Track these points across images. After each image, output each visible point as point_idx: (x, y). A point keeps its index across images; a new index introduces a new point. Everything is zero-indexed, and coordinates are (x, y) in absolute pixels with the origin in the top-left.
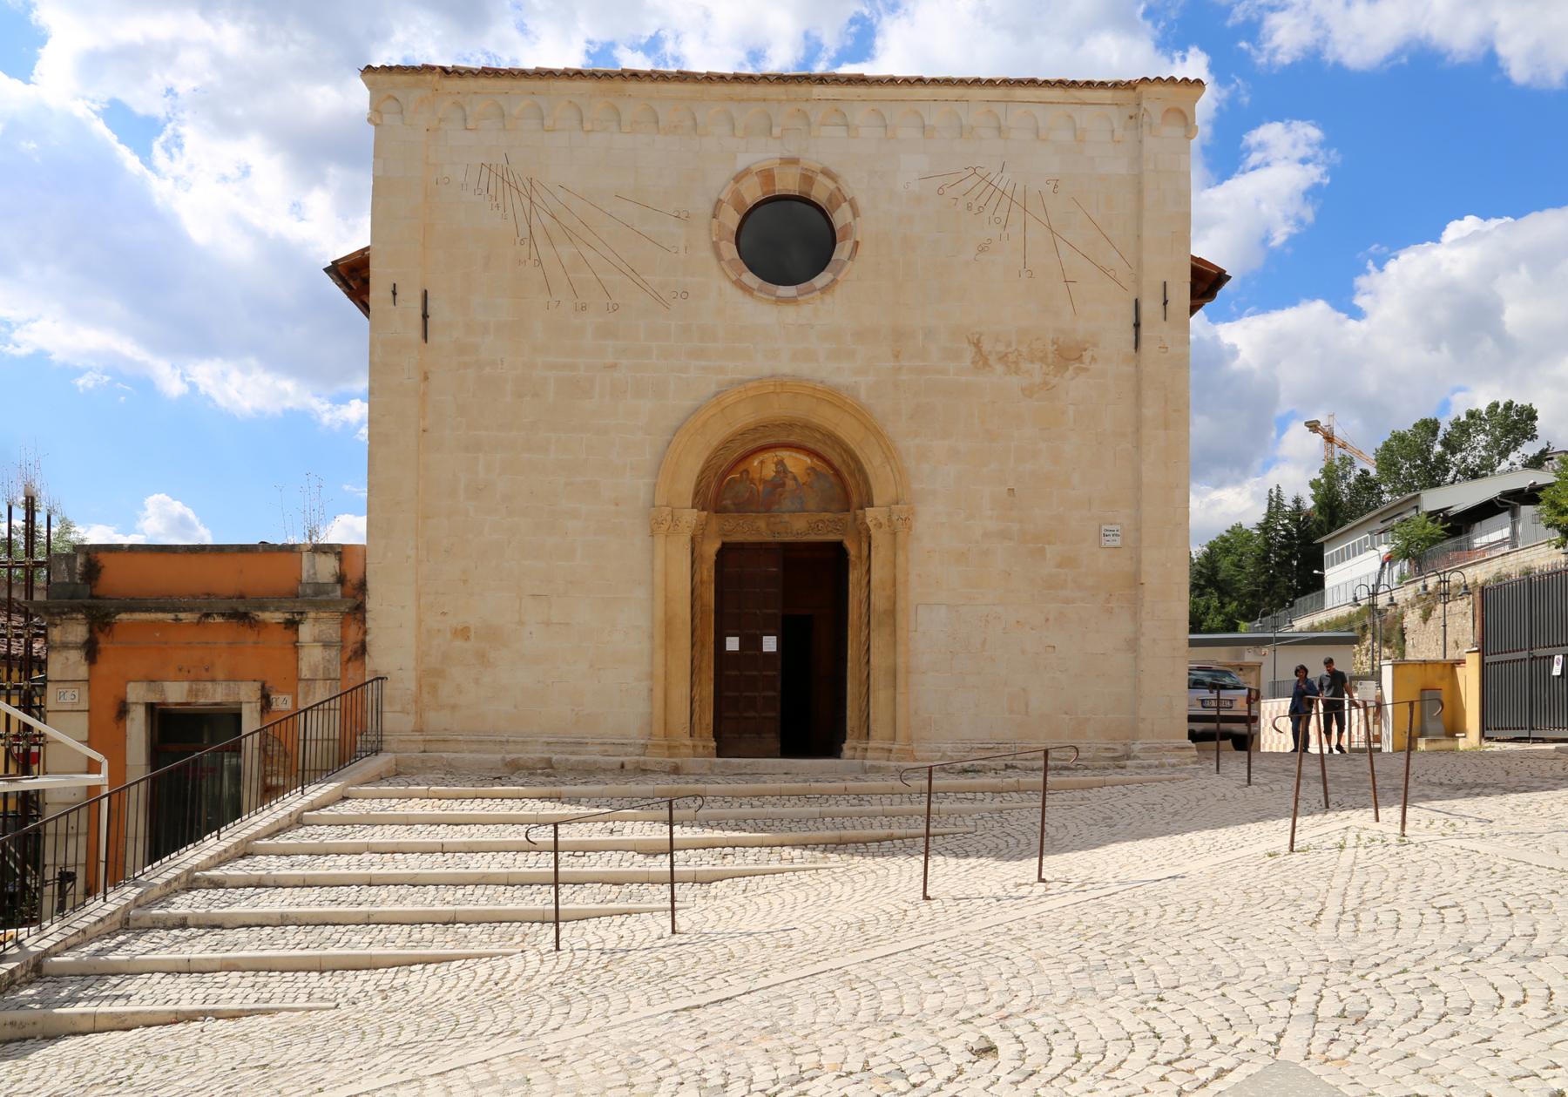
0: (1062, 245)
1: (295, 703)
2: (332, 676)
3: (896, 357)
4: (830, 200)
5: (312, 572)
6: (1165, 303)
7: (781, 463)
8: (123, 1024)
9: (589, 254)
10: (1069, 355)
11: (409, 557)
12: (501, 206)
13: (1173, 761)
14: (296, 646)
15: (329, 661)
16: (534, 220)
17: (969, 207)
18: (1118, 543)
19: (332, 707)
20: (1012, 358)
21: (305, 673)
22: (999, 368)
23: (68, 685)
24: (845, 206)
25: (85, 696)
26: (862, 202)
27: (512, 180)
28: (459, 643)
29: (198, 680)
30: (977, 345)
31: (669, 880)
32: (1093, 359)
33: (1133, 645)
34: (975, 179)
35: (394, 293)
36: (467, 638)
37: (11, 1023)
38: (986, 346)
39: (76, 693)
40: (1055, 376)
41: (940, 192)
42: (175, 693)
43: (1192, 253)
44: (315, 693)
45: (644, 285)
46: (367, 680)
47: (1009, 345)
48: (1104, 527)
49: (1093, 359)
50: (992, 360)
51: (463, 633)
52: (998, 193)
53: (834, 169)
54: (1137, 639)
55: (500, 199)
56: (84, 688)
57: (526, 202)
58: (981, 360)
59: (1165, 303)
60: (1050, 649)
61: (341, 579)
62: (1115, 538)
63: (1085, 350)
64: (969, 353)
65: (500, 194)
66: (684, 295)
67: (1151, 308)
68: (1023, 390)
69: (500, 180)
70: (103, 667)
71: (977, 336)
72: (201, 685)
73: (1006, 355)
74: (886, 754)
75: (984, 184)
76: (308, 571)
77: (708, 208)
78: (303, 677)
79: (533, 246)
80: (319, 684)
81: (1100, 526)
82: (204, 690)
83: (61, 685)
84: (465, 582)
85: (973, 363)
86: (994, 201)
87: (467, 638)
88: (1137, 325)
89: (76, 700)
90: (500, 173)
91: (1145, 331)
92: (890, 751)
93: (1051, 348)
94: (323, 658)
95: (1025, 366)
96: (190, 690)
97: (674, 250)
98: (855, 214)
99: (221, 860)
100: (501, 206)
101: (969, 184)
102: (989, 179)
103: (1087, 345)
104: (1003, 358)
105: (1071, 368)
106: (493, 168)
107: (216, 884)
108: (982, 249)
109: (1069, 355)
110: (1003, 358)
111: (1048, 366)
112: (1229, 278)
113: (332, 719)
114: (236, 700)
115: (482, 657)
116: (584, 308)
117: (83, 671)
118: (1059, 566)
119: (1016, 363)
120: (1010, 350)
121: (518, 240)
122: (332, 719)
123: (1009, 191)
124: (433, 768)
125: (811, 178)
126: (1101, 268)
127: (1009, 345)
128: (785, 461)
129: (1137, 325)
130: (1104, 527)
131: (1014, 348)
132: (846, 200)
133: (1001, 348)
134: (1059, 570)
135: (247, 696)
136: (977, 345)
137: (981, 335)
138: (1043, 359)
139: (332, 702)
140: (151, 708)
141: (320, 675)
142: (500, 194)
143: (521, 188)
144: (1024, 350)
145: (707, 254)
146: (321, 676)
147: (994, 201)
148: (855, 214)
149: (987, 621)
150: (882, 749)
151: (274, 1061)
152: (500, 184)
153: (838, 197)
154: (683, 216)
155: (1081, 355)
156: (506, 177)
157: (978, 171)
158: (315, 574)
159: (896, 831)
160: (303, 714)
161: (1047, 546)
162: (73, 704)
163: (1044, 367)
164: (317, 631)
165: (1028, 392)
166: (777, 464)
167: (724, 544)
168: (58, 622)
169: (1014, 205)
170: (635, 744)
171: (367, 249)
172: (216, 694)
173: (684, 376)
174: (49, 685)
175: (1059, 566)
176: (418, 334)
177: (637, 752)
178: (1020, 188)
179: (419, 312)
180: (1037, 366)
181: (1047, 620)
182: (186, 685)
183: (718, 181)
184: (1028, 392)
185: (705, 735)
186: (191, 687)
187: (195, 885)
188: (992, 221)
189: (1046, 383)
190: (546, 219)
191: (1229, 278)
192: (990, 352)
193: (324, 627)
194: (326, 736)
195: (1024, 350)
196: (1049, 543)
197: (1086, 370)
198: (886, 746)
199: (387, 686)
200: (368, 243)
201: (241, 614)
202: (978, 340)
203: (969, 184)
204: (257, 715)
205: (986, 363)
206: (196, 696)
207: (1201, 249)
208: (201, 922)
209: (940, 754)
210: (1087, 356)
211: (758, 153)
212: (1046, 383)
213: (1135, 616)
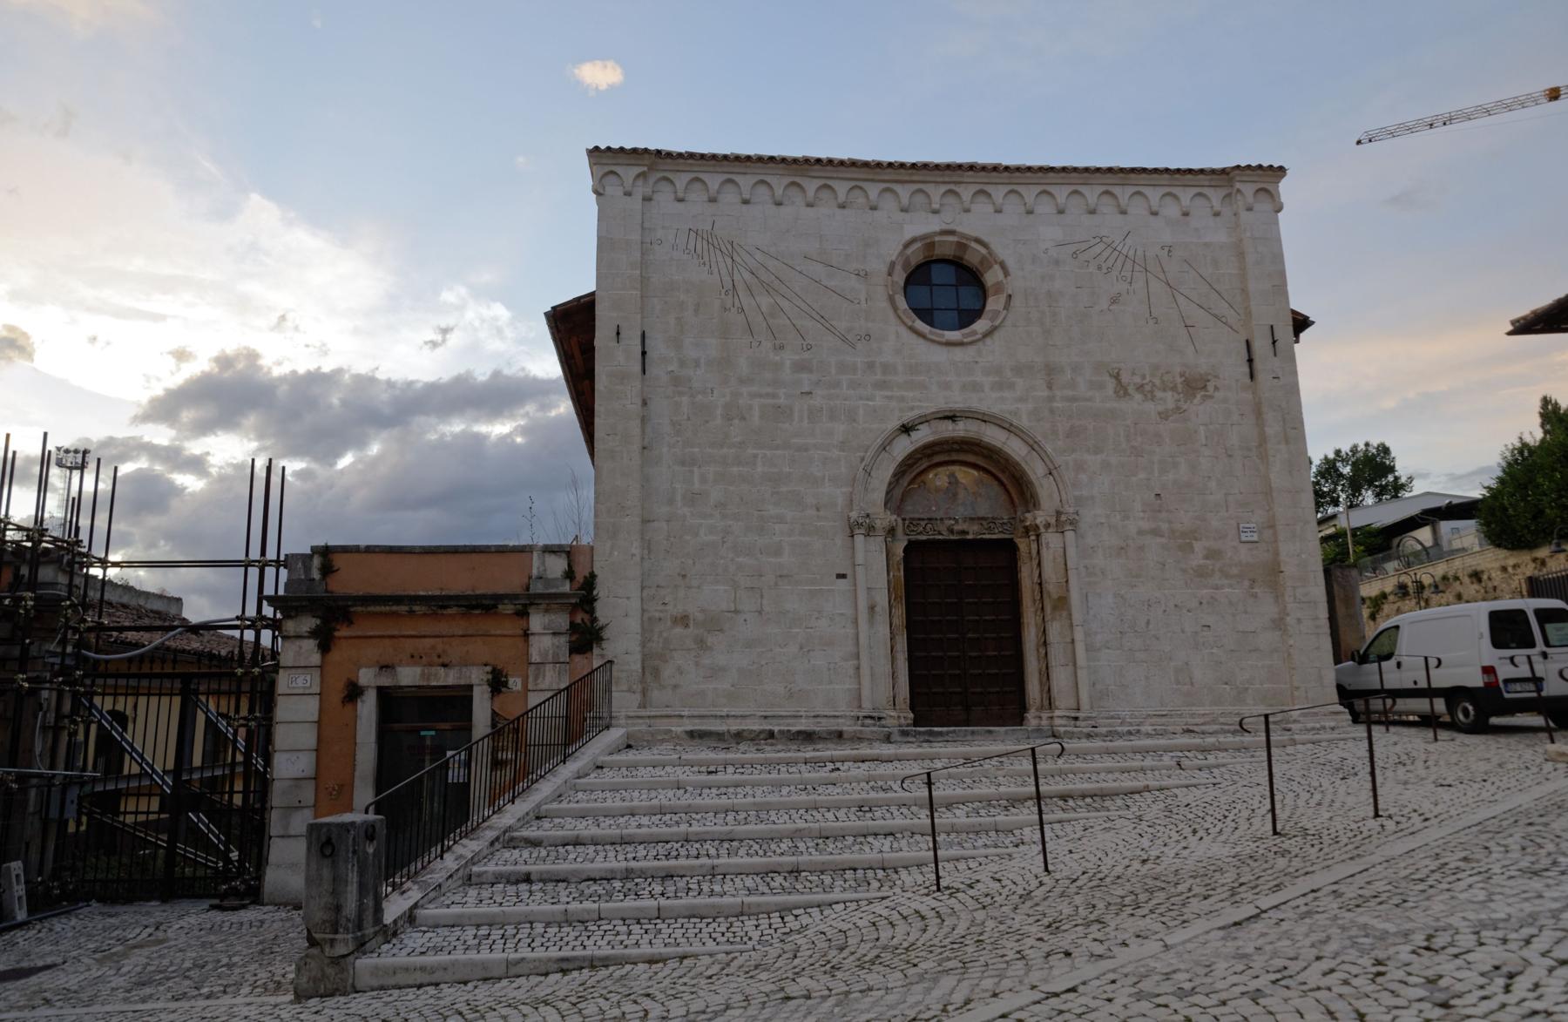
0: (1181, 299)
2: (562, 660)
3: (1050, 387)
4: (981, 263)
5: (541, 569)
6: (1274, 342)
7: (952, 475)
8: (430, 980)
9: (785, 304)
10: (1195, 385)
11: (633, 555)
12: (707, 263)
13: (1333, 724)
14: (526, 635)
15: (558, 647)
18: (1255, 538)
20: (1148, 388)
21: (535, 658)
22: (1138, 397)
23: (300, 671)
25: (317, 680)
26: (1011, 263)
27: (716, 243)
28: (679, 630)
29: (431, 665)
30: (1117, 377)
31: (930, 832)
32: (1216, 388)
33: (1279, 624)
34: (1102, 246)
35: (618, 334)
36: (687, 626)
37: (421, 969)
38: (1125, 378)
39: (308, 678)
40: (1186, 402)
41: (1075, 255)
42: (408, 676)
43: (1292, 307)
44: (544, 676)
45: (833, 330)
46: (595, 667)
47: (1144, 377)
48: (1241, 525)
49: (1216, 388)
50: (1131, 390)
51: (683, 620)
52: (1122, 258)
53: (985, 239)
54: (1282, 619)
55: (706, 259)
56: (317, 673)
57: (729, 261)
58: (1122, 391)
59: (1274, 342)
60: (1205, 629)
61: (569, 575)
63: (1209, 381)
64: (1111, 385)
65: (706, 253)
66: (867, 338)
67: (1261, 346)
68: (1159, 413)
69: (705, 243)
70: (335, 655)
72: (433, 670)
73: (1142, 386)
74: (1073, 722)
75: (1109, 250)
76: (538, 568)
77: (885, 269)
78: (533, 661)
79: (736, 297)
80: (550, 666)
81: (1238, 524)
82: (436, 675)
83: (293, 671)
84: (684, 576)
85: (1115, 392)
86: (1119, 263)
87: (687, 626)
88: (1250, 361)
89: (308, 684)
91: (1258, 364)
92: (1076, 719)
93: (1179, 380)
94: (553, 644)
95: (1159, 394)
96: (423, 675)
97: (856, 301)
98: (1006, 274)
99: (524, 821)
100: (707, 263)
101: (1097, 249)
102: (1114, 245)
103: (1209, 377)
104: (1140, 388)
105: (1199, 396)
106: (700, 232)
107: (535, 843)
108: (1114, 301)
109: (1195, 385)
110: (1140, 388)
111: (1179, 394)
112: (1313, 323)
114: (468, 682)
115: (701, 643)
116: (782, 347)
117: (316, 658)
118: (1206, 557)
120: (1144, 382)
121: (723, 291)
123: (1131, 253)
124: (663, 741)
125: (965, 245)
126: (1215, 316)
127: (1144, 377)
128: (957, 474)
129: (1250, 361)
132: (996, 262)
133: (1138, 380)
134: (1208, 562)
135: (477, 677)
136: (1117, 377)
137: (1120, 370)
138: (1174, 389)
140: (381, 691)
141: (550, 659)
142: (706, 253)
143: (723, 249)
144: (1157, 382)
145: (884, 304)
146: (551, 660)
147: (1119, 263)
148: (1006, 274)
149: (1149, 606)
150: (1068, 717)
151: (865, 955)
152: (705, 246)
153: (989, 260)
154: (862, 273)
155: (1206, 386)
157: (1104, 239)
158: (545, 570)
159: (1152, 783)
161: (1194, 542)
162: (304, 688)
163: (1176, 396)
164: (547, 621)
165: (1164, 416)
166: (949, 477)
167: (910, 542)
168: (293, 614)
169: (1137, 268)
170: (846, 716)
171: (593, 294)
172: (449, 678)
173: (871, 403)
174: (281, 671)
175: (1206, 557)
176: (638, 368)
177: (848, 723)
178: (1140, 253)
179: (639, 349)
180: (1170, 394)
181: (1201, 603)
182: (418, 670)
183: (891, 248)
184: (1164, 416)
185: (903, 706)
186: (423, 671)
187: (512, 844)
189: (1178, 408)
190: (747, 276)
191: (1313, 323)
193: (553, 617)
195: (1157, 382)
196: (1196, 539)
197: (1211, 397)
198: (1073, 715)
199: (615, 668)
200: (594, 289)
201: (482, 605)
202: (1118, 373)
203: (1097, 249)
204: (487, 695)
205: (1126, 393)
206: (428, 679)
207: (1296, 305)
208: (545, 876)
210: (1210, 386)
211: (923, 225)
212: (1178, 408)
213: (1278, 597)
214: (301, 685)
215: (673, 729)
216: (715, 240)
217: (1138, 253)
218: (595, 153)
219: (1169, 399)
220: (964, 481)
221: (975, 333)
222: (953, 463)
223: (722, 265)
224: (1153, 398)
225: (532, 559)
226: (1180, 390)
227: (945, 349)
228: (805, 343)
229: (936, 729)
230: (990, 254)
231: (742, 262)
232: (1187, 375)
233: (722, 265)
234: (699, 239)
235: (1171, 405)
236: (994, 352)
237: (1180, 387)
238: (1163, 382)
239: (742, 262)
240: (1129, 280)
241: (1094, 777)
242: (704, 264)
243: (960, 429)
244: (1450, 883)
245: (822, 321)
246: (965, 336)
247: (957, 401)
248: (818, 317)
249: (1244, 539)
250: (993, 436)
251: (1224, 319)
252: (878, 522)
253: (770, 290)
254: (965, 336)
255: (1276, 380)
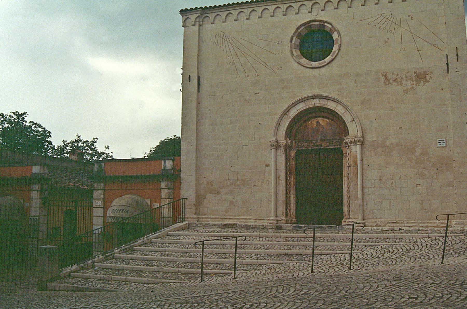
1: (160, 204)
7: (318, 122)
16: (232, 51)
17: (380, 28)
18: (444, 145)
19: (167, 207)
20: (399, 80)
24: (335, 33)
30: (386, 76)
34: (382, 18)
38: (389, 76)
57: (230, 44)
60: (418, 185)
62: (443, 143)
63: (427, 74)
64: (383, 79)
66: (281, 69)
71: (385, 73)
78: (162, 198)
86: (389, 25)
89: (100, 205)
90: (221, 36)
104: (395, 80)
105: (422, 82)
111: (413, 81)
113: (165, 214)
119: (400, 81)
122: (165, 214)
130: (438, 139)
131: (399, 76)
132: (335, 31)
133: (394, 76)
136: (386, 76)
139: (167, 205)
144: (404, 76)
147: (389, 25)
153: (334, 29)
155: (426, 77)
156: (223, 38)
160: (182, 200)
162: (100, 206)
163: (412, 82)
165: (406, 92)
166: (316, 122)
167: (298, 150)
169: (396, 25)
178: (398, 19)
184: (406, 92)
188: (389, 32)
192: (391, 78)
194: (167, 216)
195: (404, 76)
197: (428, 82)
202: (386, 74)
205: (389, 83)
209: (376, 224)
210: (428, 77)
212: (413, 88)
214: (99, 205)
215: (203, 222)
216: (225, 37)
217: (398, 20)
218: (182, 12)
219: (409, 84)
220: (322, 124)
221: (325, 62)
222: (319, 117)
223: (227, 46)
224: (401, 84)
225: (162, 163)
226: (414, 80)
227: (311, 70)
228: (257, 74)
229: (300, 225)
230: (333, 27)
231: (235, 45)
232: (417, 72)
233: (227, 46)
234: (219, 37)
235: (409, 87)
236: (333, 69)
237: (414, 78)
238: (406, 77)
239: (235, 45)
240: (393, 32)
241: (286, 248)
242: (221, 47)
243: (317, 103)
244: (383, 290)
245: (264, 64)
246: (320, 64)
247: (316, 92)
248: (262, 63)
249: (439, 146)
250: (331, 105)
251: (436, 46)
252: (281, 144)
253: (245, 55)
254: (332, 56)
255: (458, 72)
